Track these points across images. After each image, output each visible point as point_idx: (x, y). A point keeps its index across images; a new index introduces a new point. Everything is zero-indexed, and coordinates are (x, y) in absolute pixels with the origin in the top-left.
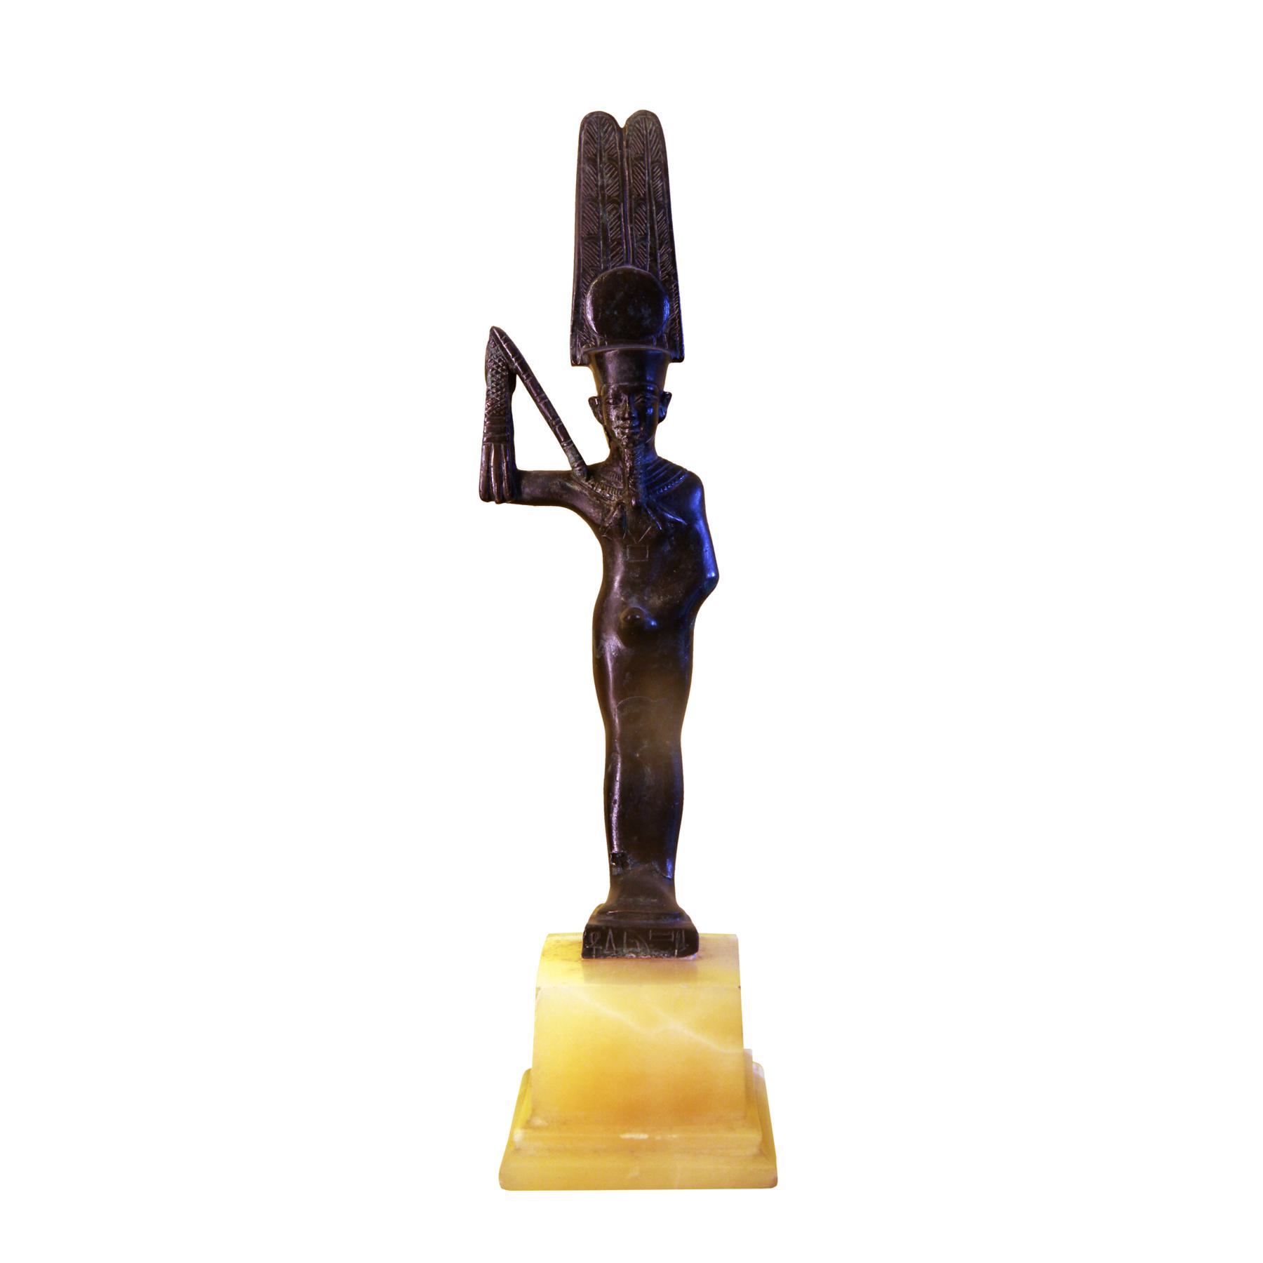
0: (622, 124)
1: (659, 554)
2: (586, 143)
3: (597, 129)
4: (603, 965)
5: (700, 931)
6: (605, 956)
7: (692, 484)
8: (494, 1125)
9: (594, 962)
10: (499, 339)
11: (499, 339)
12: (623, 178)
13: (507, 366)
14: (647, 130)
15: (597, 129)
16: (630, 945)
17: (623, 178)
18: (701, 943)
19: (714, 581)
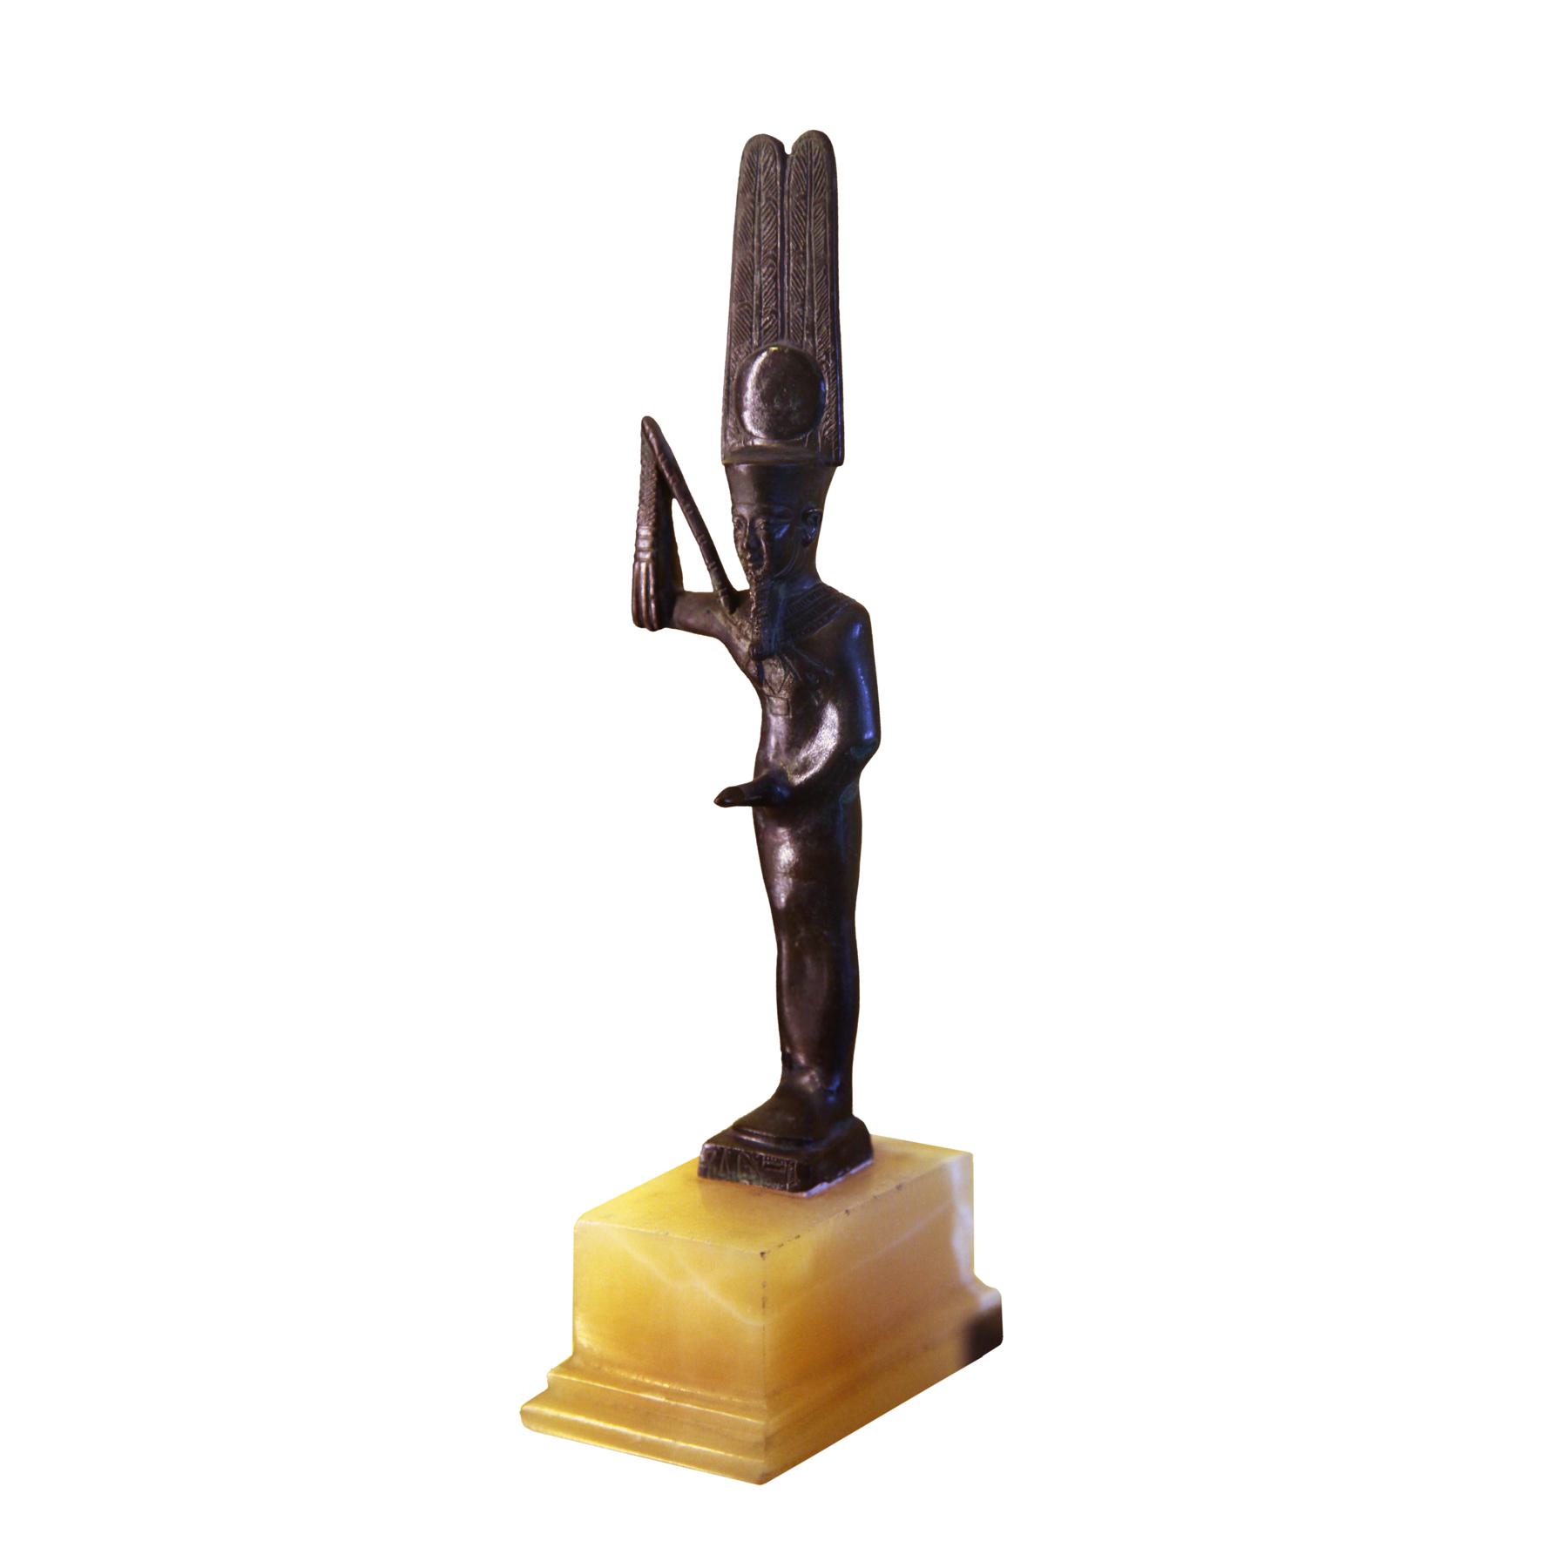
0: (788, 151)
1: (811, 650)
2: (791, 983)
3: (761, 151)
4: (713, 1185)
5: (872, 1130)
6: (720, 1178)
7: (857, 616)
8: (548, 1338)
9: (708, 1181)
10: (650, 427)
11: (650, 427)
12: (790, 202)
13: (663, 482)
14: (817, 155)
15: (761, 154)
16: (743, 1170)
17: (790, 202)
18: (876, 1153)
19: (874, 745)
